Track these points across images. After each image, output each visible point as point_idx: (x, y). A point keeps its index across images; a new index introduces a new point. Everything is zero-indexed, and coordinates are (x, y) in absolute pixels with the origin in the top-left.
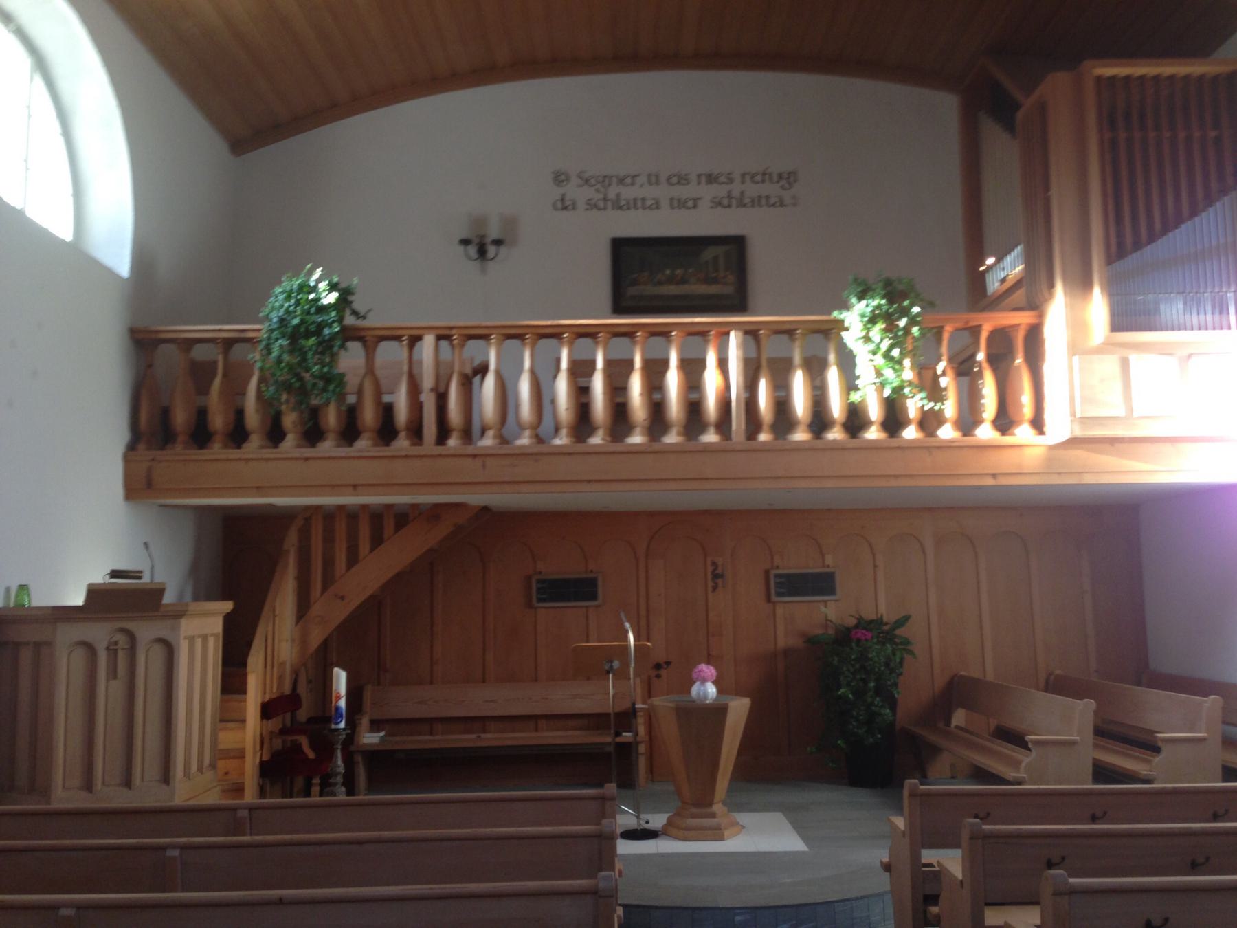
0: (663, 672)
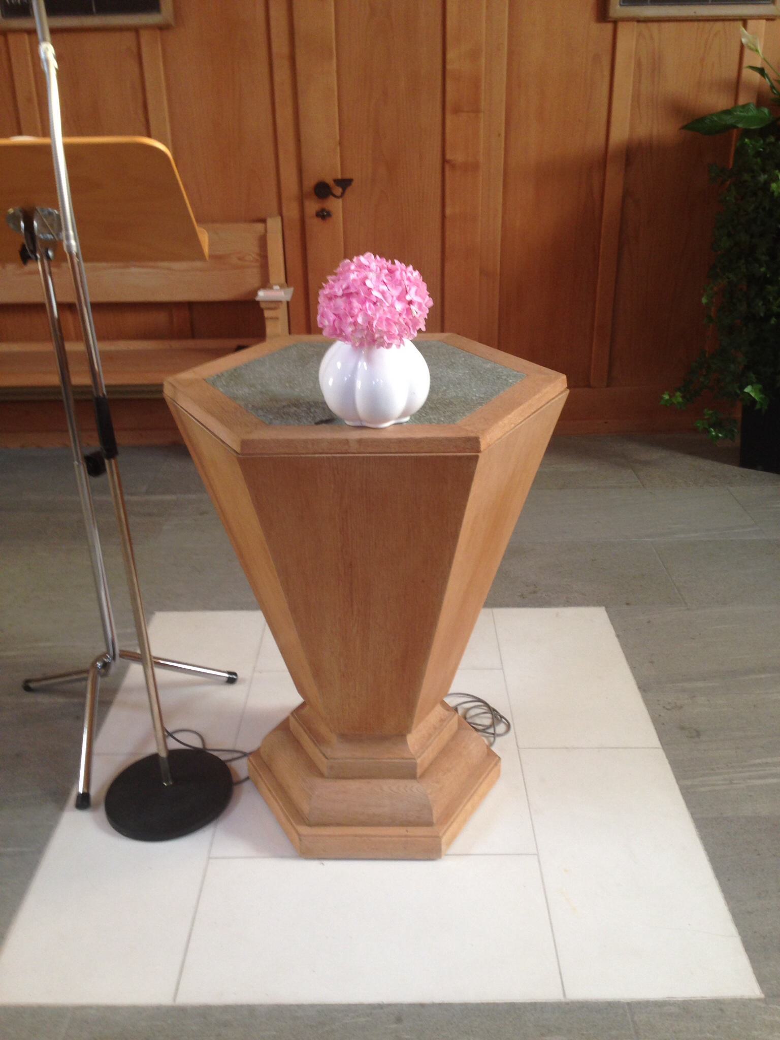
0: (336, 205)
